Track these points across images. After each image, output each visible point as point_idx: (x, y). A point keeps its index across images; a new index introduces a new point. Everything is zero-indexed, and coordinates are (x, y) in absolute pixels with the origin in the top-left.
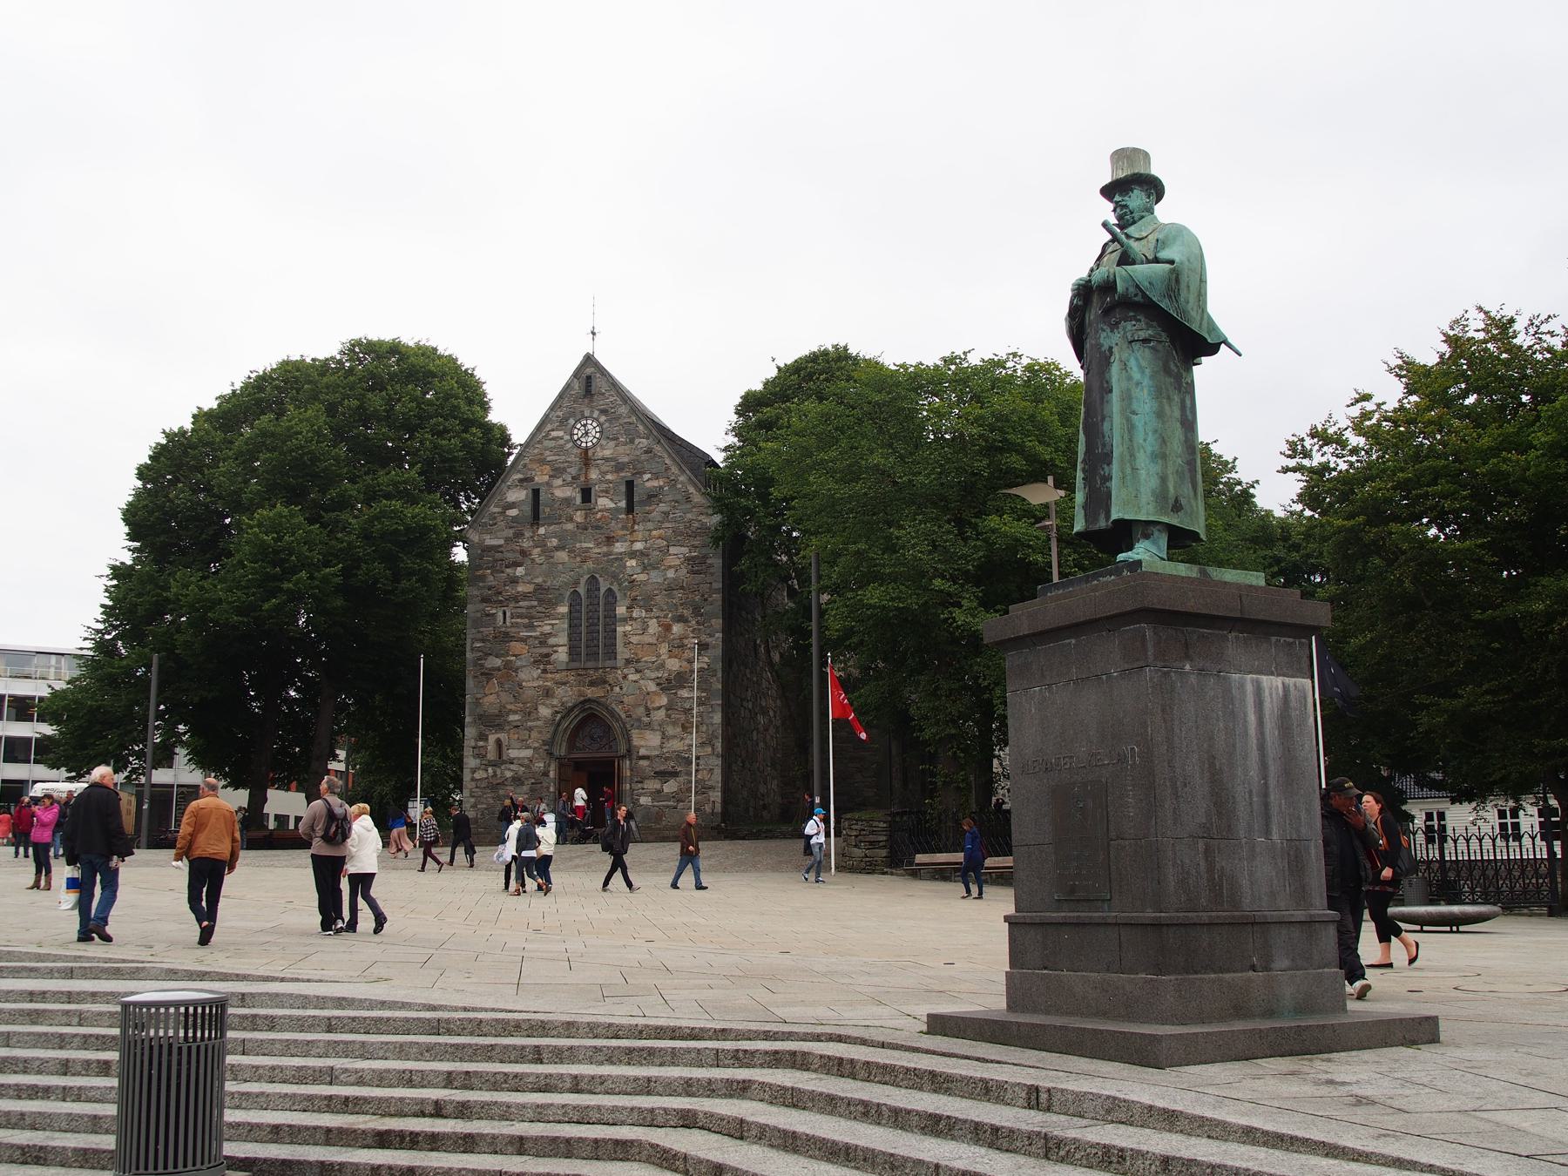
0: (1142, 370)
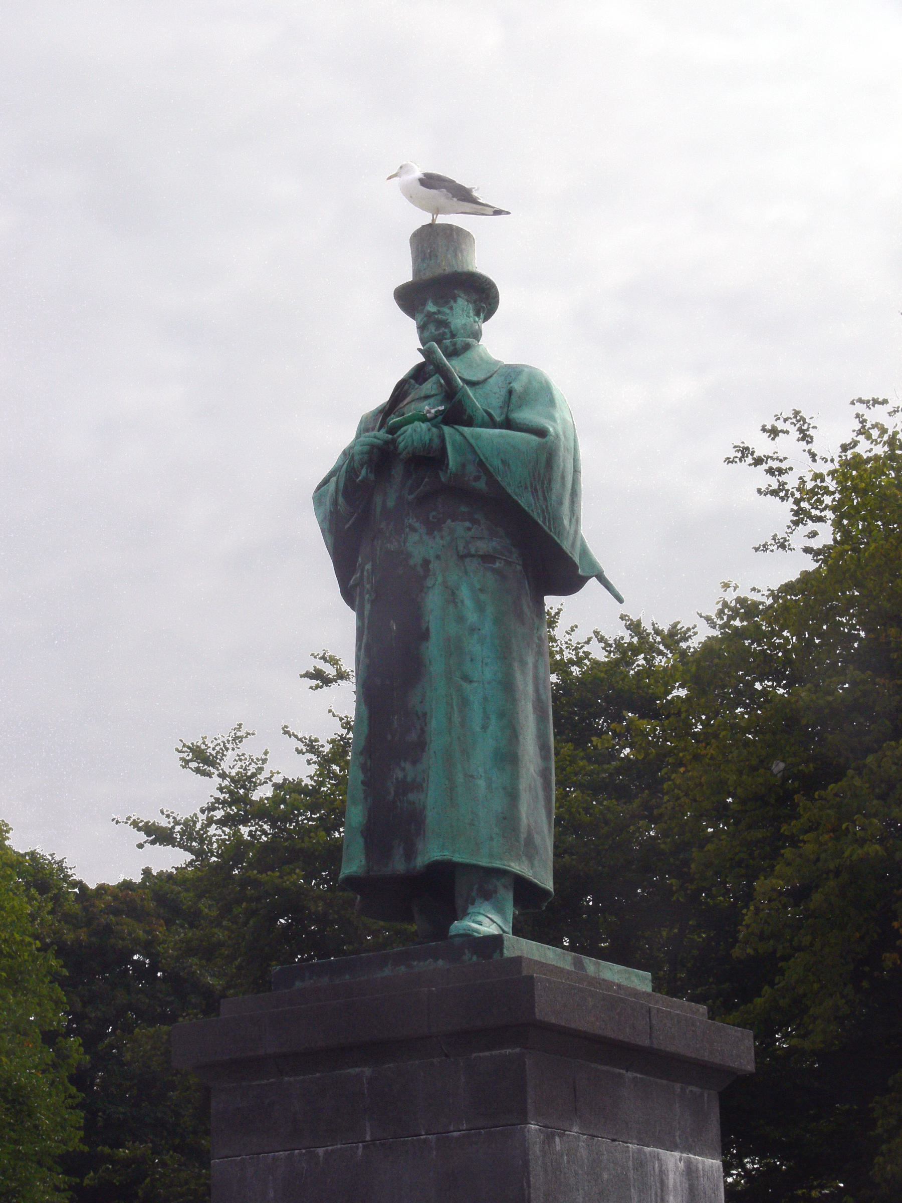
0: (480, 608)
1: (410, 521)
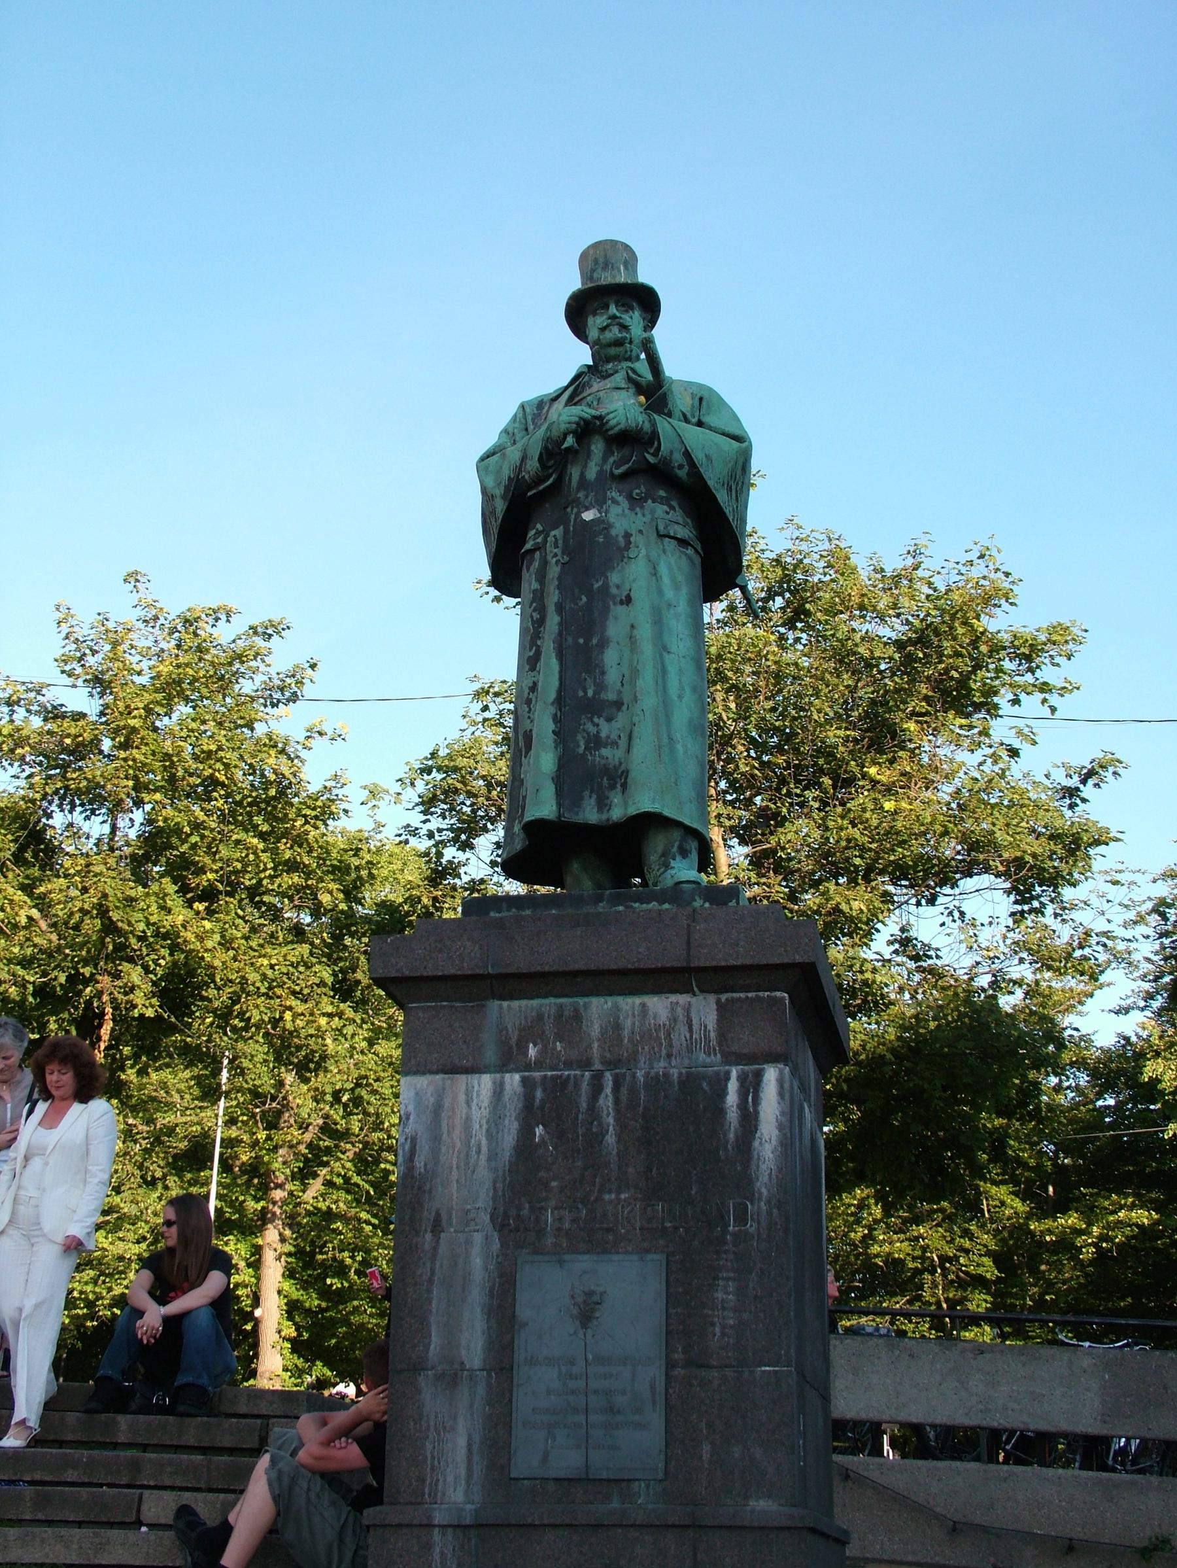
0: (677, 588)
1: (613, 494)
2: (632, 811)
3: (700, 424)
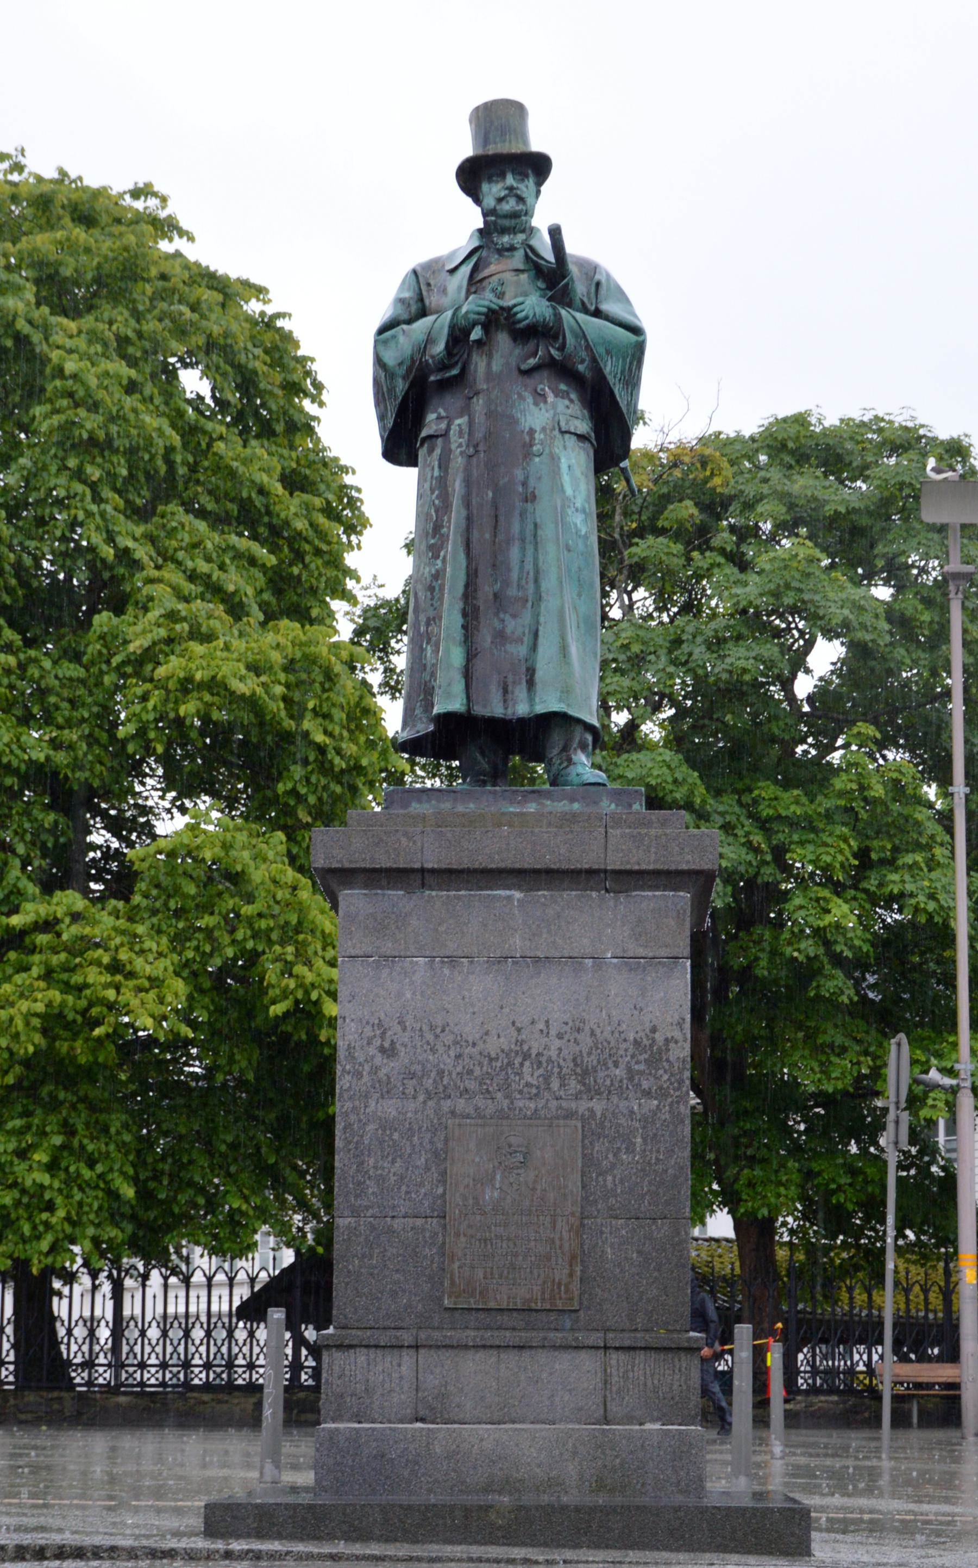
2: (540, 709)
3: (597, 313)
